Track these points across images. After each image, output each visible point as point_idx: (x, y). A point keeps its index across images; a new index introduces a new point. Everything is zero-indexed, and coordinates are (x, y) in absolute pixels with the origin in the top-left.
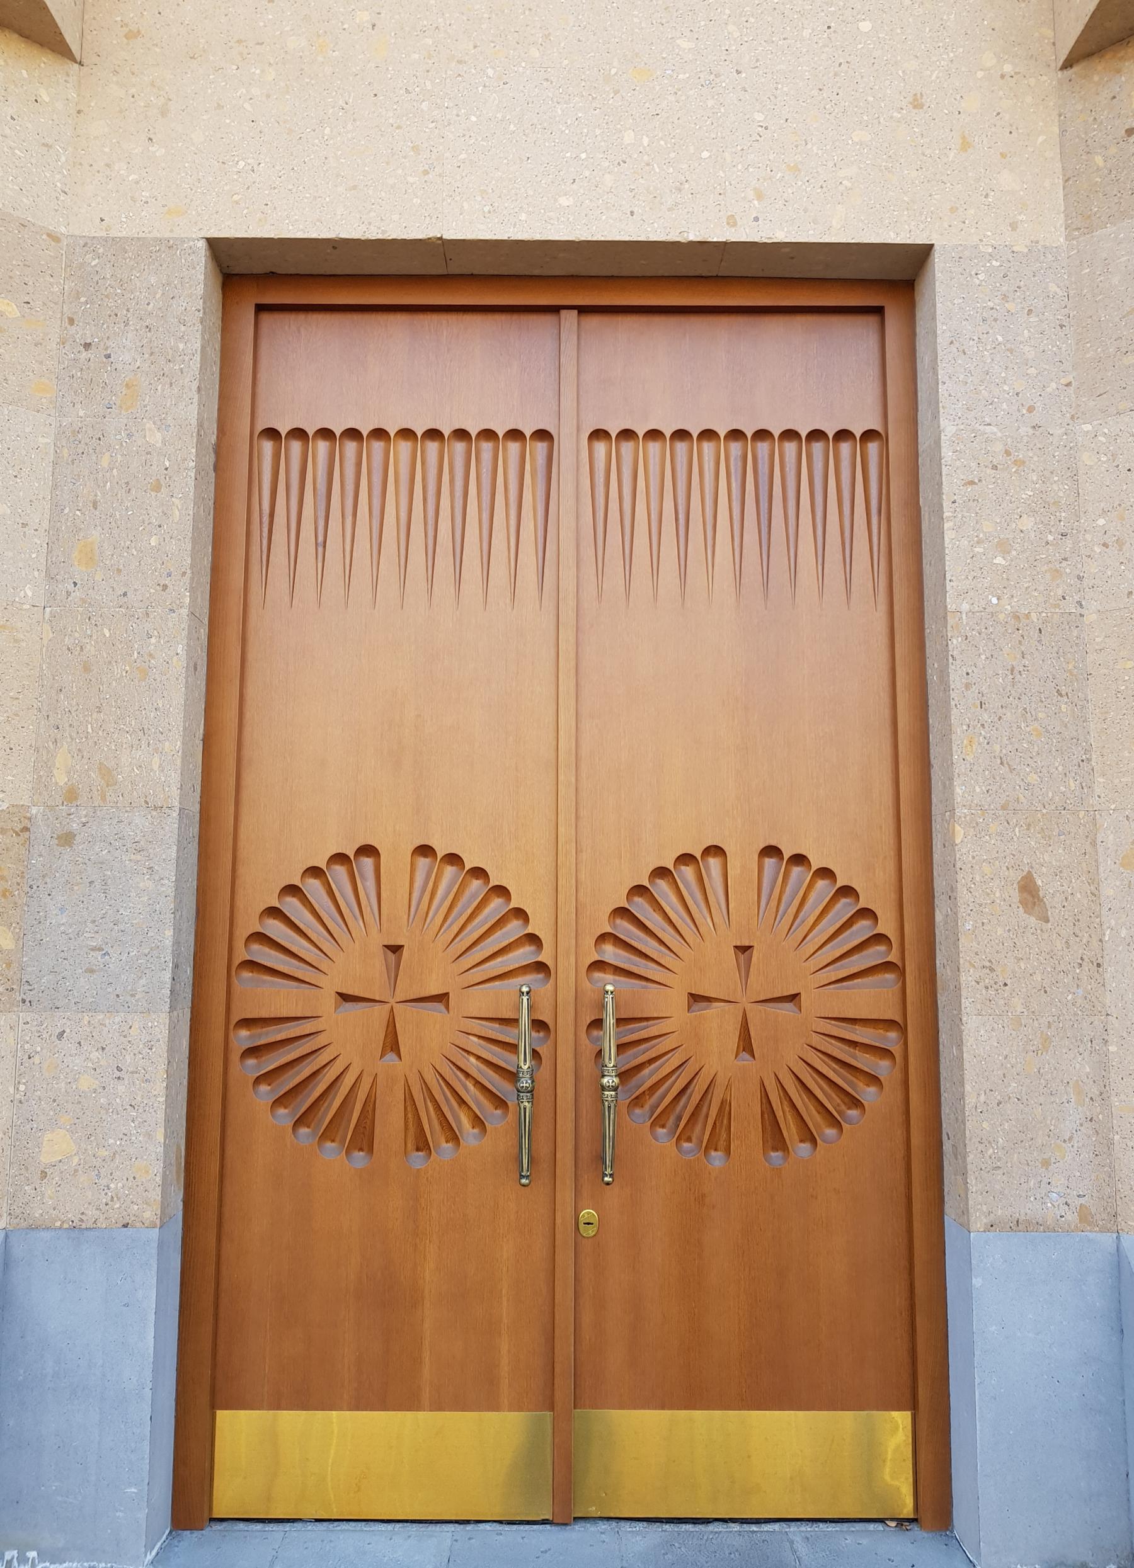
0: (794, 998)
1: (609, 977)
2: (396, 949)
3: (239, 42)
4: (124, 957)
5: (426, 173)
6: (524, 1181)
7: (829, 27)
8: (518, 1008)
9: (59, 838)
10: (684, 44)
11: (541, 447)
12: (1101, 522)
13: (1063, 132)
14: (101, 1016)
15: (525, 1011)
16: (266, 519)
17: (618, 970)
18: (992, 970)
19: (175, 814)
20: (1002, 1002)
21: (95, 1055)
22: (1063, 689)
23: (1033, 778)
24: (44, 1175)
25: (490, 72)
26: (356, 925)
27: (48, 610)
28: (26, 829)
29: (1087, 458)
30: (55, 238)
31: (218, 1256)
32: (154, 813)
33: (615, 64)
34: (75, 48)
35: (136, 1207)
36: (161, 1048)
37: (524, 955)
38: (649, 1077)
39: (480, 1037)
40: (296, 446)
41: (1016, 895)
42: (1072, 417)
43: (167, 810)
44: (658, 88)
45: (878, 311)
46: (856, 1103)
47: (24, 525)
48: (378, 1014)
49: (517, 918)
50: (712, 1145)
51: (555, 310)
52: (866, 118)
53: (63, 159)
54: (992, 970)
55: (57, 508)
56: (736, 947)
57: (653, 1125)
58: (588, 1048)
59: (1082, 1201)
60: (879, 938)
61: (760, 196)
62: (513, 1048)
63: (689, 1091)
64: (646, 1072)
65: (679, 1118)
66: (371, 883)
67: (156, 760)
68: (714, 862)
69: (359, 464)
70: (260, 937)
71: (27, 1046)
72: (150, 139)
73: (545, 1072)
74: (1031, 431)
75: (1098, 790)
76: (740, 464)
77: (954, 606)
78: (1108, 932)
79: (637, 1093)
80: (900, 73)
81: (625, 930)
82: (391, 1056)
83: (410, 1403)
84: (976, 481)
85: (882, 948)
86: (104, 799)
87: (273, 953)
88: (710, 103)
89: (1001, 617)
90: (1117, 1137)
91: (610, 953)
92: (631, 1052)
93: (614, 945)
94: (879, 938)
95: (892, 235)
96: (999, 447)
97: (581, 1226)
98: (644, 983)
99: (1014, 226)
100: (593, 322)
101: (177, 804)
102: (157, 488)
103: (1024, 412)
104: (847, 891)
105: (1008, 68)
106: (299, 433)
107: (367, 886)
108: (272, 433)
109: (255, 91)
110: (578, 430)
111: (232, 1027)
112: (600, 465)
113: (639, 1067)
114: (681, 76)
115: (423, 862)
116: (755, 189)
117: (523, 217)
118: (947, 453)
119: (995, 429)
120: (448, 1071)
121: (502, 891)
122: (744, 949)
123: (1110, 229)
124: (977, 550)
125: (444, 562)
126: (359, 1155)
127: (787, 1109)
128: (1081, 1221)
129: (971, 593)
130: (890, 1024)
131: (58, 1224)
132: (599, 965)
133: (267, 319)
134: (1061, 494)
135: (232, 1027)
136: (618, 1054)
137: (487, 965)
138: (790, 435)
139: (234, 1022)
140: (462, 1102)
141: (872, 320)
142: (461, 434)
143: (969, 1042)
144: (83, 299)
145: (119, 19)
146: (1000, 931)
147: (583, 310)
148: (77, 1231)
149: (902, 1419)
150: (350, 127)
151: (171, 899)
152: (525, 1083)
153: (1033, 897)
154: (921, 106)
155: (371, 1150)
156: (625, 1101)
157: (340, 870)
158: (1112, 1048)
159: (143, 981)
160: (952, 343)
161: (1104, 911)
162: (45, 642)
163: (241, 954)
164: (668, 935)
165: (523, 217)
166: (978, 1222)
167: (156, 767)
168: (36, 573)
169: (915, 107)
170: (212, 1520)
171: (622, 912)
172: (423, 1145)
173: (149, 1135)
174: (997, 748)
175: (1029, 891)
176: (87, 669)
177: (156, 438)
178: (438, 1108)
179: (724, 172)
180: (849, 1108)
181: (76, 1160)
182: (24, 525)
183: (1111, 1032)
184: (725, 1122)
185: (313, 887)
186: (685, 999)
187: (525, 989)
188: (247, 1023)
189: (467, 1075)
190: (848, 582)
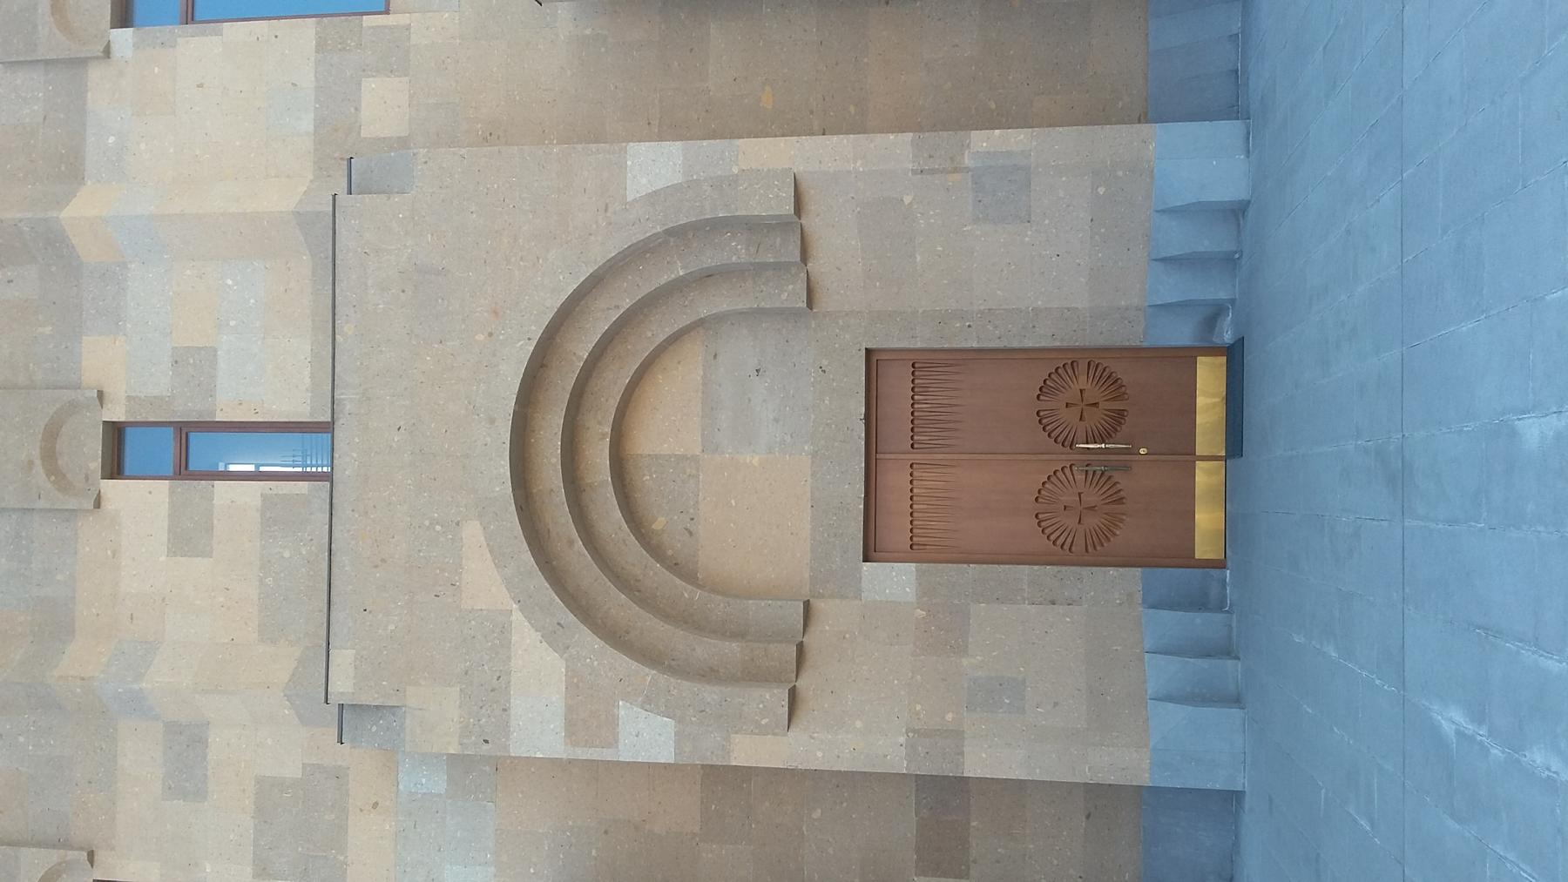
70: (1062, 547)
157: (1044, 421)
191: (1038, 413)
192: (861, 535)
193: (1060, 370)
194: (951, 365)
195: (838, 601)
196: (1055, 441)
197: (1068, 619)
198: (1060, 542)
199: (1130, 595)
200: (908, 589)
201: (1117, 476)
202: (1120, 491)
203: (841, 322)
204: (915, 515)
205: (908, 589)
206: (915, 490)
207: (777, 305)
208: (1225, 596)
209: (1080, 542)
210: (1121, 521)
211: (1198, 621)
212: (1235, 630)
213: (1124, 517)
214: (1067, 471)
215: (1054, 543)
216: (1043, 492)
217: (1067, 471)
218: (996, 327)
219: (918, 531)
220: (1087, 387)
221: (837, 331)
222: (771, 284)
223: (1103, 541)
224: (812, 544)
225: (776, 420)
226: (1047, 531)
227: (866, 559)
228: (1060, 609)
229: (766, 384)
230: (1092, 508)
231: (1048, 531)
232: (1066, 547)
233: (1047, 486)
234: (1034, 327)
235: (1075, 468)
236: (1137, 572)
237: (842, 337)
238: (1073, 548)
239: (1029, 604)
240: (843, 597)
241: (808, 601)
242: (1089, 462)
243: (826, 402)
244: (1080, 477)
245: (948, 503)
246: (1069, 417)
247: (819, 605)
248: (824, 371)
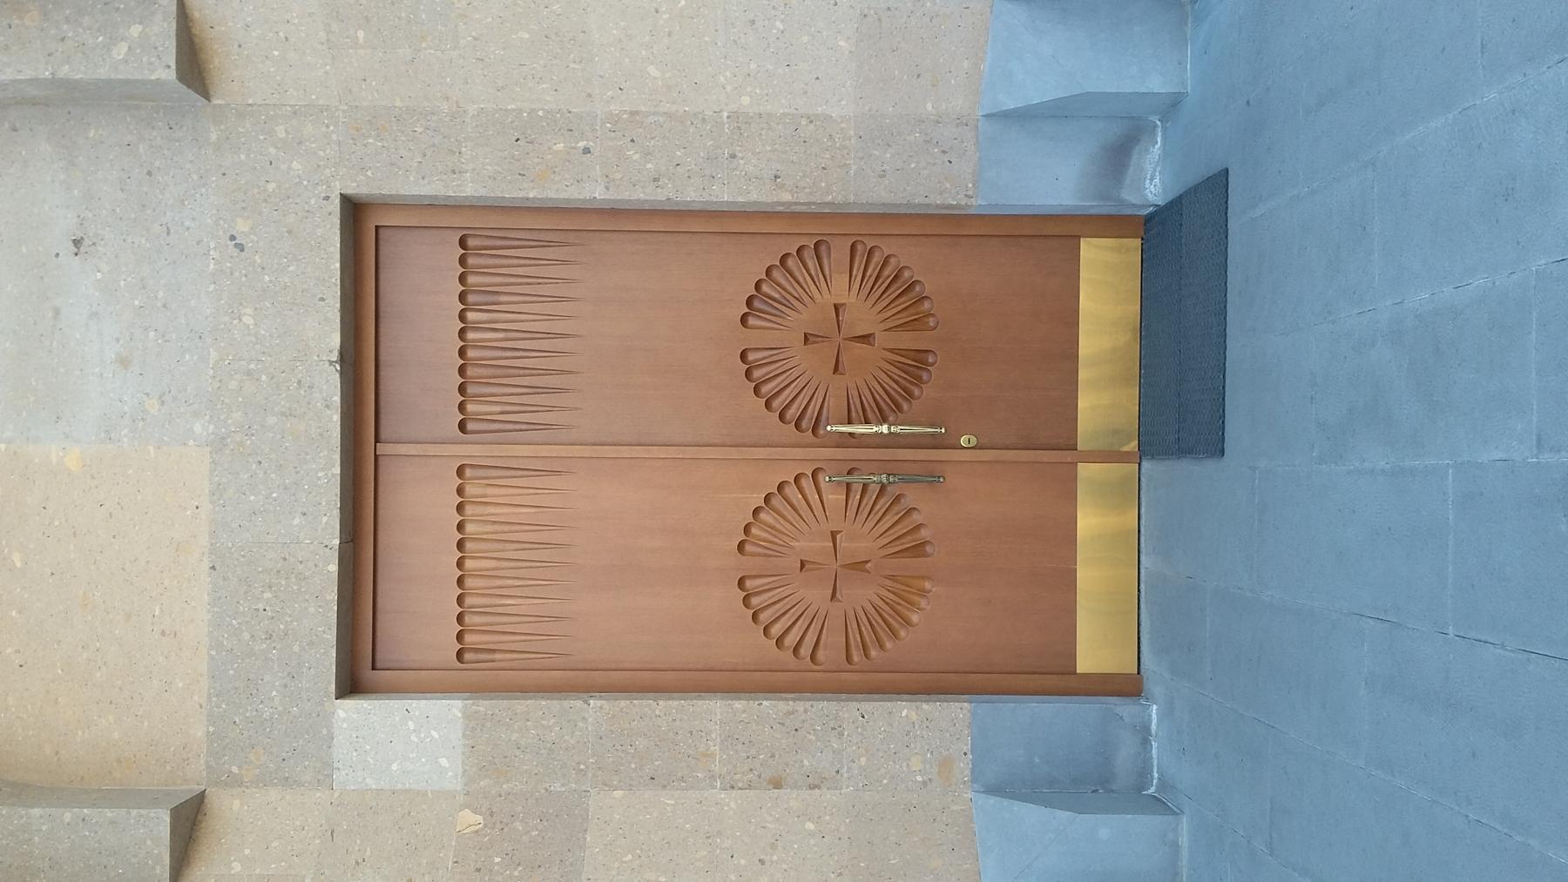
8: (839, 483)
11: (468, 472)
56: (805, 344)
68: (751, 357)
70: (796, 650)
95: (332, 249)
97: (969, 446)
133: (378, 665)
139: (849, 666)
141: (381, 231)
142: (460, 508)
147: (377, 441)
157: (757, 374)
170: (1139, 673)
186: (837, 376)
191: (743, 356)
192: (331, 636)
193: (790, 262)
194: (548, 244)
195: (274, 794)
196: (782, 417)
197: (810, 826)
198: (791, 640)
199: (946, 764)
200: (444, 762)
201: (912, 496)
202: (918, 527)
203: (281, 132)
204: (469, 582)
205: (444, 762)
206: (469, 528)
207: (103, 73)
208: (1147, 762)
209: (833, 642)
210: (923, 593)
211: (1104, 833)
212: (1185, 853)
213: (927, 585)
214: (807, 484)
215: (779, 642)
216: (754, 531)
217: (807, 484)
218: (647, 154)
219: (477, 619)
220: (850, 299)
221: (272, 150)
222: (86, 20)
223: (881, 634)
224: (212, 658)
225: (124, 362)
226: (764, 617)
227: (351, 684)
228: (793, 798)
229: (99, 275)
230: (859, 566)
231: (765, 617)
232: (805, 651)
233: (763, 516)
234: (733, 156)
235: (823, 479)
236: (958, 711)
237: (284, 167)
238: (821, 655)
239: (722, 789)
240: (287, 782)
241: (200, 798)
242: (854, 465)
243: (247, 320)
244: (834, 497)
245: (544, 555)
246: (807, 364)
247: (228, 807)
248: (241, 247)
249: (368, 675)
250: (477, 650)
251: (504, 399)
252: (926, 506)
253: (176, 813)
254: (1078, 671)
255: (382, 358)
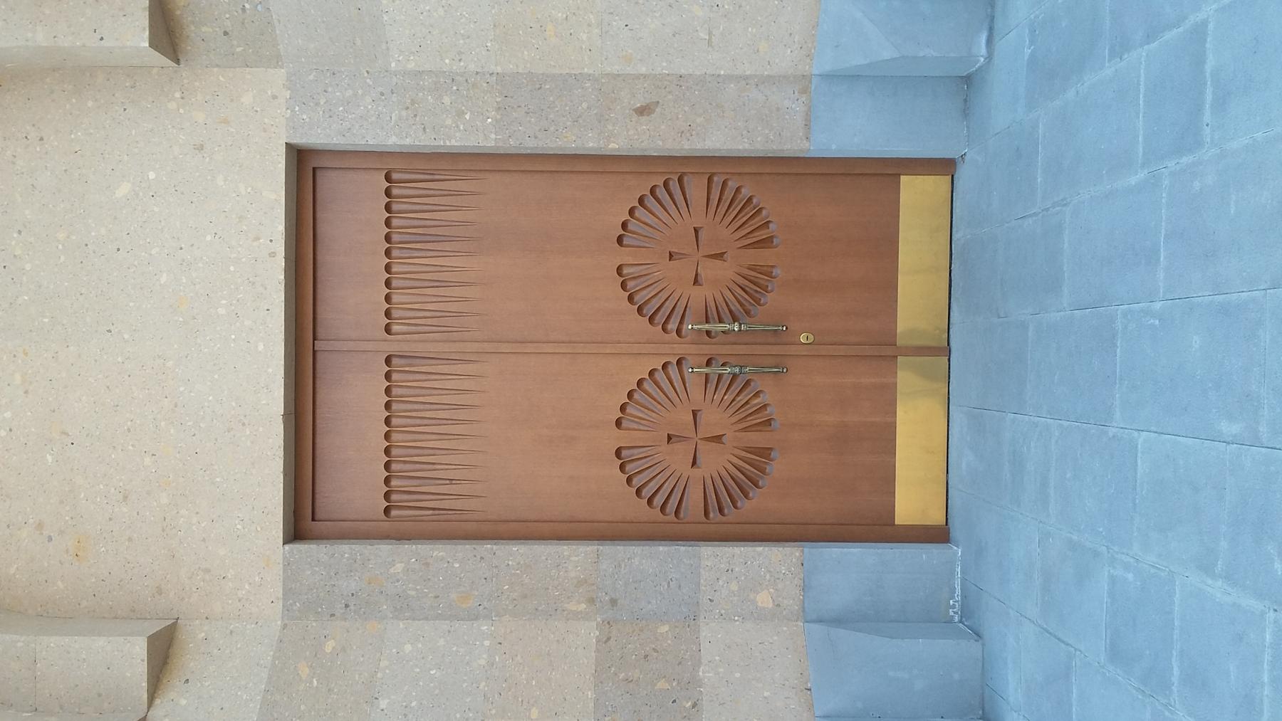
0: (696, 230)
1: (685, 327)
2: (669, 438)
3: (163, 530)
4: (673, 570)
5: (244, 424)
6: (785, 370)
7: (153, 196)
9: (613, 606)
10: (164, 279)
11: (395, 361)
12: (447, 61)
13: (217, 66)
14: (702, 581)
15: (702, 370)
16: (437, 512)
17: (681, 322)
18: (683, 132)
19: (601, 548)
20: (699, 128)
21: (721, 582)
22: (538, 86)
23: (585, 105)
24: (778, 605)
25: (182, 389)
26: (658, 458)
27: (494, 619)
28: (609, 623)
29: (411, 66)
30: (285, 627)
31: (821, 524)
32: (601, 558)
33: (176, 318)
34: (170, 622)
35: (794, 560)
36: (716, 549)
37: (673, 371)
38: (735, 307)
39: (714, 394)
40: (394, 497)
41: (644, 119)
42: (387, 71)
43: (600, 552)
44: (192, 295)
45: (314, 169)
46: (750, 199)
47: (449, 632)
48: (703, 446)
49: (653, 375)
50: (770, 275)
51: (314, 352)
52: (209, 177)
53: (237, 625)
54: (683, 132)
55: (439, 617)
56: (670, 260)
57: (759, 305)
58: (721, 338)
59: (796, 92)
60: (666, 184)
61: (257, 239)
62: (720, 376)
63: (743, 286)
64: (733, 308)
65: (756, 291)
66: (636, 451)
67: (573, 558)
69: (405, 462)
71: (716, 617)
72: (224, 578)
73: (732, 360)
74: (395, 95)
75: (591, 72)
76: (405, 251)
77: (493, 142)
78: (664, 71)
79: (744, 313)
80: (181, 156)
81: (660, 318)
82: (724, 439)
83: (893, 426)
84: (423, 126)
85: (671, 183)
86: (593, 584)
87: (671, 501)
88: (200, 265)
89: (498, 117)
90: (766, 73)
91: (672, 326)
92: (723, 315)
93: (668, 324)
94: (666, 184)
95: (280, 165)
96: (404, 113)
97: (808, 342)
98: (688, 309)
99: (275, 97)
100: (321, 332)
101: (596, 547)
102: (427, 564)
103: (383, 97)
104: (641, 201)
105: (178, 95)
106: (387, 496)
107: (637, 453)
108: (387, 511)
109: (195, 520)
110: (385, 341)
111: (708, 521)
112: (405, 328)
113: (731, 311)
114: (184, 281)
115: (625, 424)
116: (253, 241)
117: (270, 370)
118: (408, 141)
119: (394, 115)
120: (731, 411)
121: (640, 383)
122: (671, 256)
123: (281, 47)
124: (462, 128)
125: (461, 415)
126: (773, 454)
127: (752, 235)
128: (806, 93)
129: (486, 132)
130: (710, 180)
131: (801, 597)
132: (679, 332)
133: (318, 516)
134: (430, 80)
135: (708, 521)
136: (724, 323)
137: (678, 390)
138: (388, 223)
140: (747, 403)
141: (319, 173)
142: (388, 406)
143: (718, 146)
144: (320, 610)
145: (149, 599)
146: (663, 127)
147: (315, 339)
148: (805, 588)
149: (902, 177)
150: (216, 467)
151: (644, 548)
152: (737, 370)
153: (646, 109)
154: (202, 146)
155: (771, 449)
156: (748, 320)
157: (628, 468)
158: (722, 73)
159: (685, 560)
160: (344, 136)
161: (654, 72)
162: (511, 619)
163: (672, 517)
164: (664, 296)
165: (270, 370)
166: (805, 145)
167: (577, 559)
168: (475, 625)
169: (202, 149)
170: (946, 525)
171: (651, 320)
172: (768, 422)
173: (760, 554)
174: (569, 123)
175: (643, 111)
176: (525, 597)
177: (399, 567)
178: (750, 414)
179: (242, 258)
180: (752, 203)
181: (771, 590)
182: (449, 632)
183: (714, 73)
184: (758, 267)
185: (637, 482)
187: (690, 370)
188: (706, 514)
189: (733, 400)
190: (473, 193)
209: (694, 499)
249: (308, 523)
250: (398, 477)
251: (418, 421)
252: (770, 391)
253: (152, 640)
254: (896, 523)
255: (318, 488)
